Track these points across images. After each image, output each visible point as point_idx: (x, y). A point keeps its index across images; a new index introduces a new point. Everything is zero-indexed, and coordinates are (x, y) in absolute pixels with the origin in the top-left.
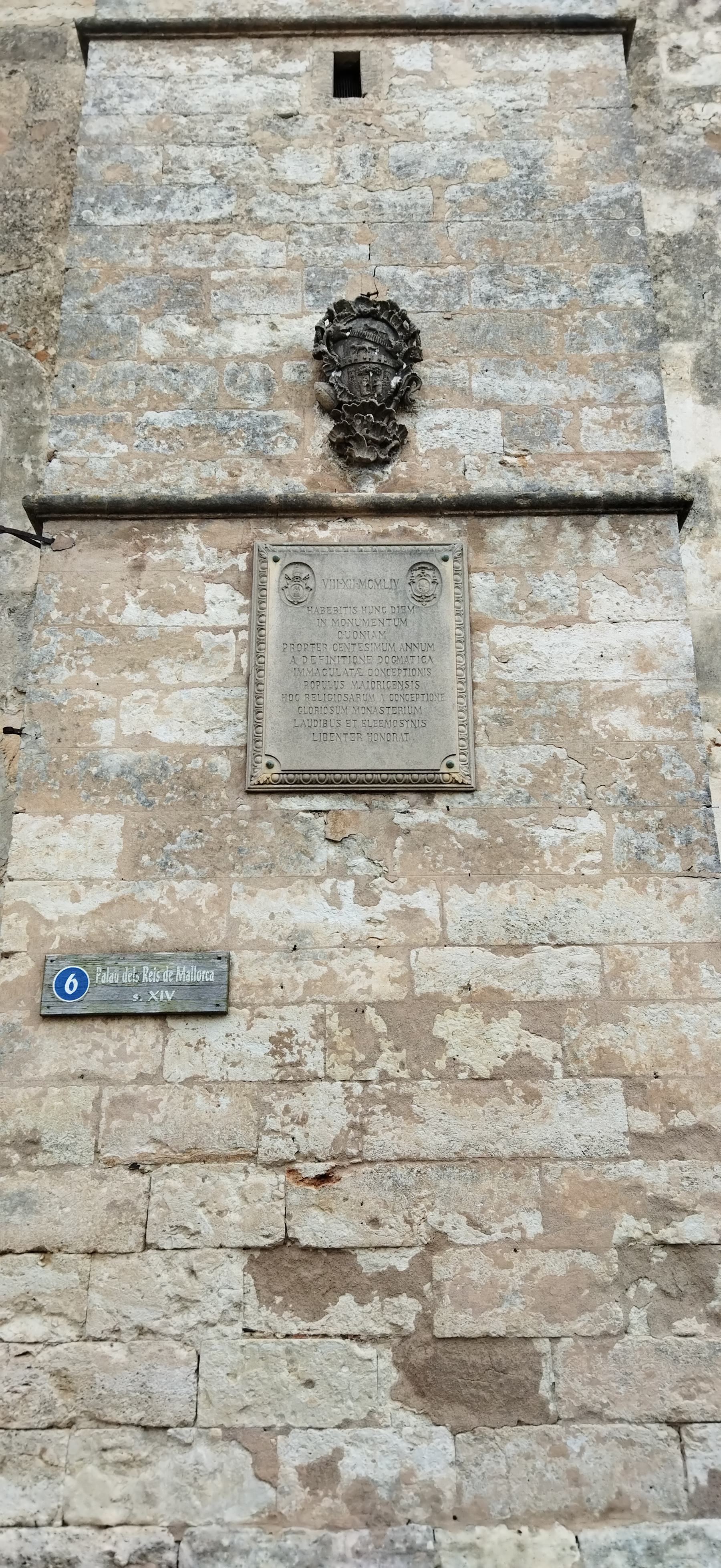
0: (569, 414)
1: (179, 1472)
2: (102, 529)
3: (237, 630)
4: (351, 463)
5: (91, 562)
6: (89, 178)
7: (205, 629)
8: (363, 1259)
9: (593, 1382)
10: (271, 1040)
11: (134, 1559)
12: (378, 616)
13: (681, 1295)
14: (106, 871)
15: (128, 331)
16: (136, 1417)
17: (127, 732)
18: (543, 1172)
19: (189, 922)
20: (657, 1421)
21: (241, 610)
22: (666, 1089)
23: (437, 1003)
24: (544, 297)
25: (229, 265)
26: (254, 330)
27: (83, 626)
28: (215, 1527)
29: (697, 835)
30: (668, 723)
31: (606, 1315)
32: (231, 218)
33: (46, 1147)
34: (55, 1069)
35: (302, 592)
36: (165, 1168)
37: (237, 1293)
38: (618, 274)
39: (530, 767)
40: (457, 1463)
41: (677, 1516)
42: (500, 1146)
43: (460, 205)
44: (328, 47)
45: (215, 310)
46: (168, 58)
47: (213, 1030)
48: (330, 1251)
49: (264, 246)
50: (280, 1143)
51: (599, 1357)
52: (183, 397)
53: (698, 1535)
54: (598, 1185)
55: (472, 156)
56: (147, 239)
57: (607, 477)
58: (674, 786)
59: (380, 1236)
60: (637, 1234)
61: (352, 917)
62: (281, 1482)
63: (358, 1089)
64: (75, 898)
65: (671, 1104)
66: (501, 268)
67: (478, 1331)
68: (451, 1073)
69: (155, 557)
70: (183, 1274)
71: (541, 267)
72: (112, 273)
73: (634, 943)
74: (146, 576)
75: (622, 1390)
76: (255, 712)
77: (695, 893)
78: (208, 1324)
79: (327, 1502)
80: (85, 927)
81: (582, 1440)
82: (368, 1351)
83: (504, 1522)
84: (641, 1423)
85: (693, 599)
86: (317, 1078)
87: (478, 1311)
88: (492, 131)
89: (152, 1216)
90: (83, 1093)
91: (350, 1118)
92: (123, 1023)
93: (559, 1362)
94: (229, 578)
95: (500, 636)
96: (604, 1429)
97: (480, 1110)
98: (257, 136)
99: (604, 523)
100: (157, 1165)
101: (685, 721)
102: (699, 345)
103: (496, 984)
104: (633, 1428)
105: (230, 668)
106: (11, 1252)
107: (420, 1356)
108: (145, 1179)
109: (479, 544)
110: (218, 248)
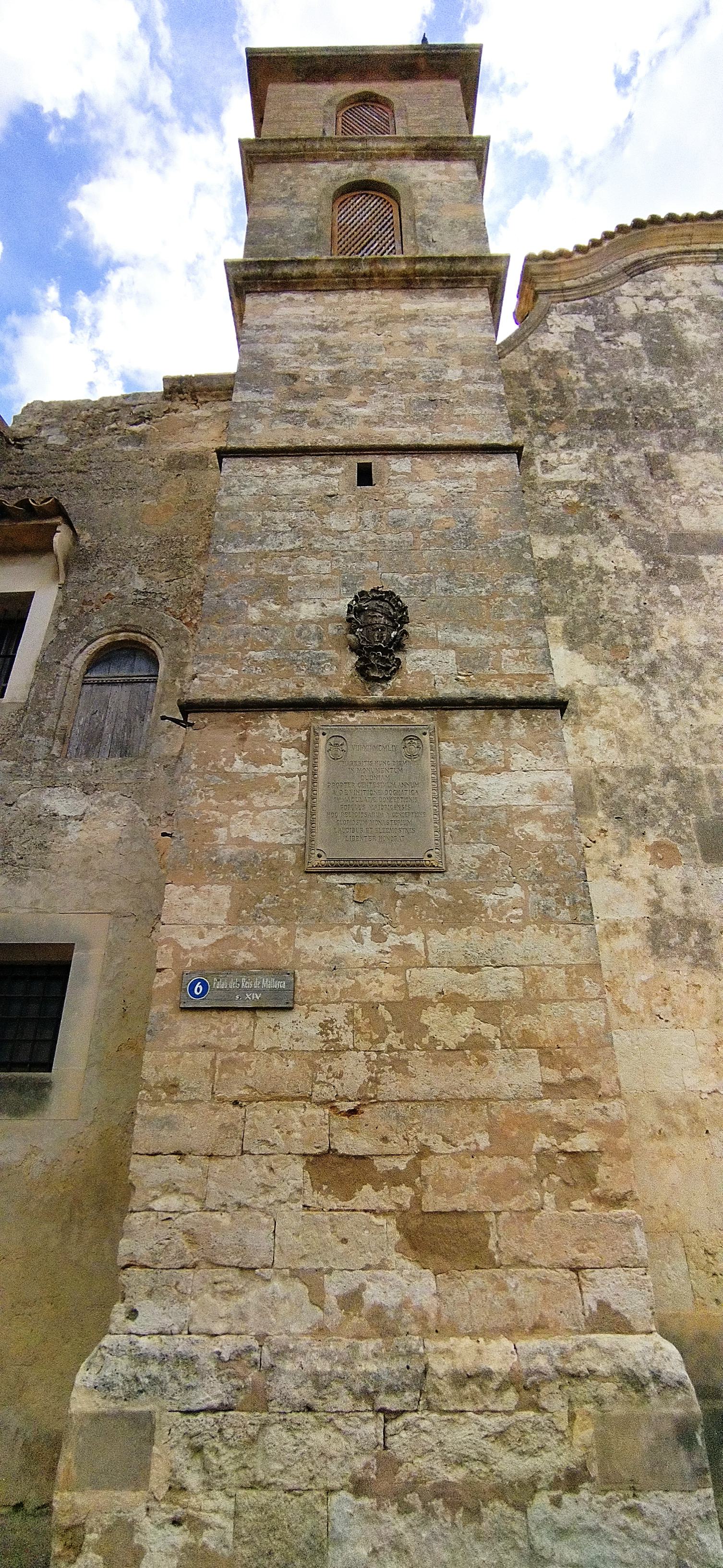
0: (494, 653)
1: (262, 1298)
2: (222, 717)
3: (300, 775)
4: (369, 679)
5: (215, 736)
6: (221, 528)
7: (282, 775)
8: (377, 1162)
9: (522, 1241)
10: (321, 1025)
11: (233, 1357)
12: (386, 766)
13: (576, 1184)
14: (220, 920)
15: (241, 608)
16: (235, 1261)
17: (234, 836)
18: (490, 1107)
19: (270, 951)
20: (563, 1267)
21: (303, 763)
22: (564, 1056)
23: (423, 1003)
24: (478, 590)
25: (299, 573)
26: (312, 607)
27: (209, 773)
28: (285, 1336)
29: (579, 899)
30: (559, 831)
31: (529, 1196)
32: (300, 549)
33: (182, 1089)
34: (189, 1041)
35: (340, 753)
36: (255, 1104)
37: (299, 1183)
38: (519, 578)
39: (478, 857)
40: (437, 1294)
41: (579, 1332)
42: (462, 1092)
43: (429, 542)
44: (355, 460)
45: (290, 596)
46: (269, 468)
47: (285, 1019)
48: (357, 1157)
49: (319, 563)
50: (325, 1089)
51: (525, 1225)
52: (271, 643)
53: (592, 1345)
54: (522, 1115)
55: (434, 516)
56: (253, 560)
57: (518, 688)
58: (564, 869)
59: (388, 1148)
60: (548, 1146)
61: (370, 949)
62: (326, 1306)
63: (374, 1056)
64: (201, 936)
65: (567, 1065)
66: (453, 573)
67: (450, 1208)
68: (432, 1047)
69: (253, 733)
70: (265, 1170)
71: (475, 574)
72: (233, 578)
73: (543, 965)
74: (247, 743)
75: (541, 1246)
76: (310, 823)
77: (579, 934)
78: (281, 1202)
79: (356, 1320)
80: (207, 953)
81: (516, 1279)
82: (381, 1221)
83: (469, 1335)
84: (554, 1269)
85: (570, 760)
86: (348, 1049)
87: (449, 1195)
88: (446, 503)
89: (246, 1133)
90: (204, 1057)
91: (370, 1074)
92: (229, 1013)
93: (501, 1228)
94: (296, 745)
95: (459, 779)
96: (530, 1272)
97: (450, 1069)
98: (315, 506)
99: (517, 713)
100: (250, 1102)
101: (569, 830)
102: (566, 618)
103: (459, 991)
104: (548, 1272)
105: (296, 798)
106: (161, 1154)
107: (414, 1224)
108: (243, 1110)
109: (444, 725)
110: (293, 564)
